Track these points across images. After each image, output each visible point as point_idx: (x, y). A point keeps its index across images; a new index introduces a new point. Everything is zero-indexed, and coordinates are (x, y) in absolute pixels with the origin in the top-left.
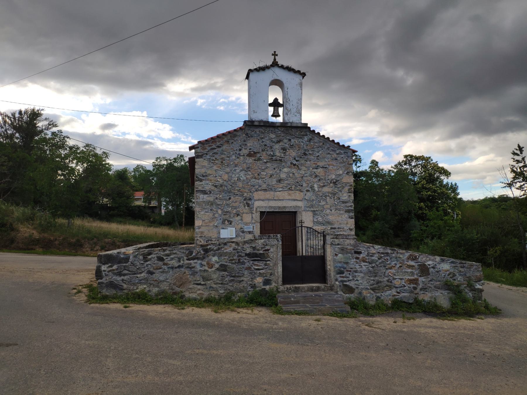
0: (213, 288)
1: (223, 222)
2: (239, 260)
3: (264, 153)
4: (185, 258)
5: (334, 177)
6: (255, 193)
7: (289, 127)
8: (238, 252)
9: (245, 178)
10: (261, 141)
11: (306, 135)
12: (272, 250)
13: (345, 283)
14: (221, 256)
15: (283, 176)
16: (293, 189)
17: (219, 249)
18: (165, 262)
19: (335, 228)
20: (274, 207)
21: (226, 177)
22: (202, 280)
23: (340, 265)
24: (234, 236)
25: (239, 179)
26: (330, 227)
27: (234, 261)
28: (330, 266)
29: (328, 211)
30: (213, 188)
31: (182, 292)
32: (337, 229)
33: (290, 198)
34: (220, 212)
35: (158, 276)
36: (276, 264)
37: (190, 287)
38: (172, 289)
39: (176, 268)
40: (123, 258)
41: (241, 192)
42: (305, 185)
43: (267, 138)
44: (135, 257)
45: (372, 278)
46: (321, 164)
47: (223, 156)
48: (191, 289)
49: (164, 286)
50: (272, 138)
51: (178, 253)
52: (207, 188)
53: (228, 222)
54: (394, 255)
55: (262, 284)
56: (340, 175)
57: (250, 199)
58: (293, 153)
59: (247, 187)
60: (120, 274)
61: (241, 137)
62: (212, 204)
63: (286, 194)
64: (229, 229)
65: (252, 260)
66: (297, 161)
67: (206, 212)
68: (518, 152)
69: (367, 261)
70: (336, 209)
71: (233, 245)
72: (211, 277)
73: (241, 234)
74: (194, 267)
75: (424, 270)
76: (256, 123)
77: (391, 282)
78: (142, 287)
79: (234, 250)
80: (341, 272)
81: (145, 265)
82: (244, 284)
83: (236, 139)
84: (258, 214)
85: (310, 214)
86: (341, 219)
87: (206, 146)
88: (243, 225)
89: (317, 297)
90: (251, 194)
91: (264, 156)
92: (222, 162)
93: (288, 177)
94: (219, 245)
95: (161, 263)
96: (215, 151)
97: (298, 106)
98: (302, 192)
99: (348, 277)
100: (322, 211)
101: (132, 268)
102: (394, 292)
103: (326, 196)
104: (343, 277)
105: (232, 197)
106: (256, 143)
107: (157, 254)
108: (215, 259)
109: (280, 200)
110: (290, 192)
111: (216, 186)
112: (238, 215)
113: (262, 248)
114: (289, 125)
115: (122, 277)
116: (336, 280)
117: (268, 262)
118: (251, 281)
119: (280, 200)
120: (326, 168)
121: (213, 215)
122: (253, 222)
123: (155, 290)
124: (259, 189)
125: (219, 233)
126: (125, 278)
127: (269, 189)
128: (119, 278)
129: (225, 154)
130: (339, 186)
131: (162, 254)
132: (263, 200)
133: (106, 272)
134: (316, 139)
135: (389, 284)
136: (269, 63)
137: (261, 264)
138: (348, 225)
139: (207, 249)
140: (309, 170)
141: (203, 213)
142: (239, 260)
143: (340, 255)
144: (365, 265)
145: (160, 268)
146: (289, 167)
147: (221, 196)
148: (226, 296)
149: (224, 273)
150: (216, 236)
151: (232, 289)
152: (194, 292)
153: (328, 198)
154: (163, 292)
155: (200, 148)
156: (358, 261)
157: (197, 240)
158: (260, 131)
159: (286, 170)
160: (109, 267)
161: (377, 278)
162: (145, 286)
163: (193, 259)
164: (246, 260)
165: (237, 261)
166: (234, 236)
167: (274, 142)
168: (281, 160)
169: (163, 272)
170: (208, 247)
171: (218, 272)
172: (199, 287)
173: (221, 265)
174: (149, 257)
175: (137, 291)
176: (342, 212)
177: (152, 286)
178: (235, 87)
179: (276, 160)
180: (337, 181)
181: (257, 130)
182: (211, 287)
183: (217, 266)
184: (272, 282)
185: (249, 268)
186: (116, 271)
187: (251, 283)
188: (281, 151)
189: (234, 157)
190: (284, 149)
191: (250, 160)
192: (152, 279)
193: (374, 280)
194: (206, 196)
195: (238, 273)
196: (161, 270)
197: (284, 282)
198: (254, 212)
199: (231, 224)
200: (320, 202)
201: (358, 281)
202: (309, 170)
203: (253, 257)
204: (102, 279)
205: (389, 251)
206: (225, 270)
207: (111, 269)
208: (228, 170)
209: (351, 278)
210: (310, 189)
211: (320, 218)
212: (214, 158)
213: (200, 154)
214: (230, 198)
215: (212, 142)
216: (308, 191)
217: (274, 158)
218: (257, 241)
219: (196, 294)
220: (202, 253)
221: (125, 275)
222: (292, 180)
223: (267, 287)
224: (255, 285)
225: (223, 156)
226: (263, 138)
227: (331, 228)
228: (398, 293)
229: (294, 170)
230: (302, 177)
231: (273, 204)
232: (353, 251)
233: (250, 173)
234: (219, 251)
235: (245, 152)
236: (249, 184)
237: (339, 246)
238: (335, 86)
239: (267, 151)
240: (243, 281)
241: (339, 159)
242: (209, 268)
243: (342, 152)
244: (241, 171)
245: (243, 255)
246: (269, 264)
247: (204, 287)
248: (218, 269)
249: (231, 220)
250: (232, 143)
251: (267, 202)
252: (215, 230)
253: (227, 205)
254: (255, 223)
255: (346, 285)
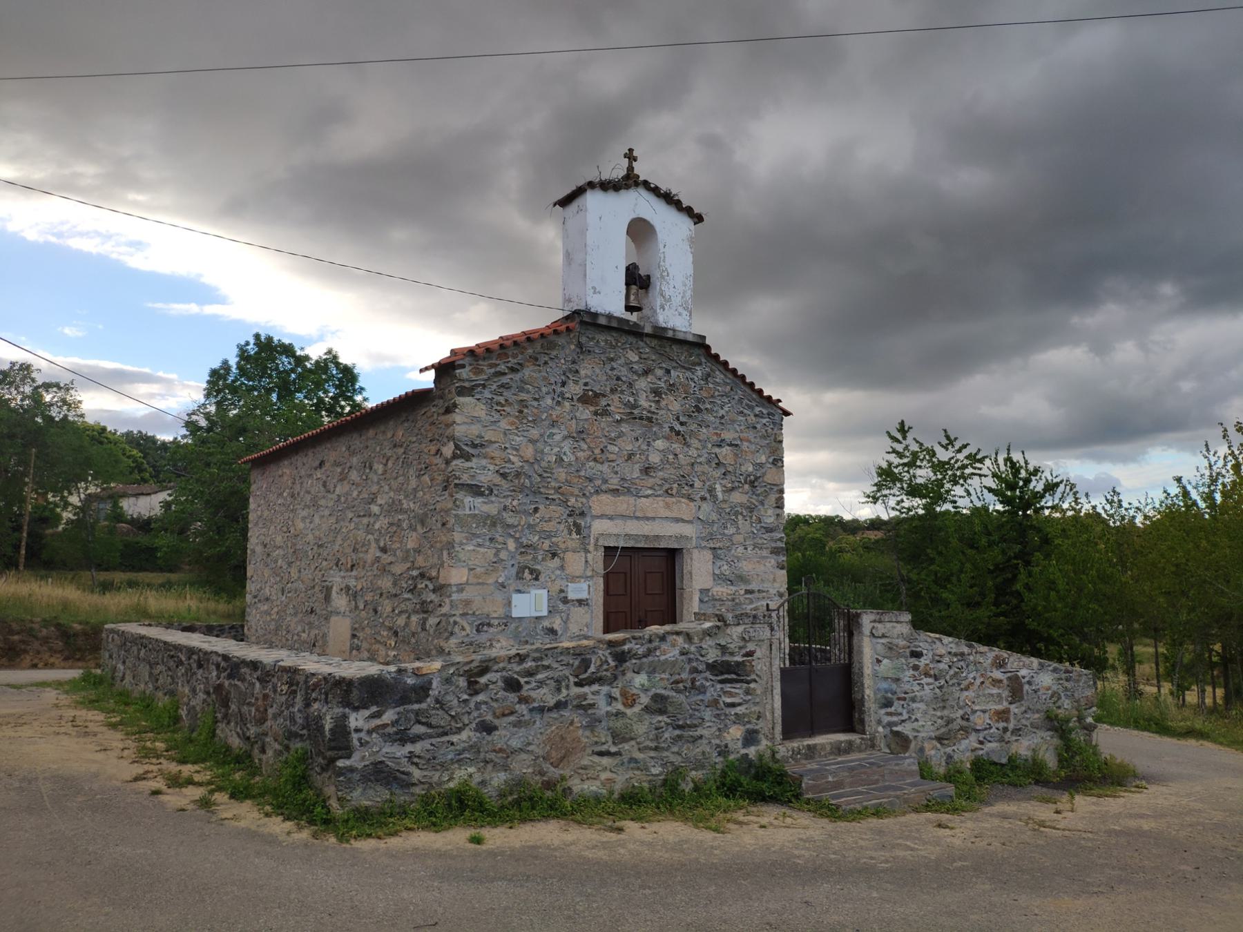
0: (636, 761)
1: (519, 576)
2: (693, 681)
3: (616, 397)
4: (572, 679)
5: (751, 469)
6: (594, 498)
7: (669, 339)
8: (690, 660)
9: (573, 458)
10: (608, 367)
11: (700, 364)
12: (758, 654)
13: (895, 729)
14: (654, 671)
15: (655, 458)
16: (674, 492)
17: (649, 652)
18: (524, 693)
19: (751, 592)
20: (636, 537)
21: (529, 452)
22: (610, 743)
23: (884, 685)
24: (545, 613)
25: (560, 460)
26: (744, 587)
27: (681, 685)
28: (870, 690)
29: (741, 549)
30: (498, 480)
31: (563, 778)
32: (757, 595)
33: (668, 514)
34: (511, 545)
35: (507, 737)
36: (769, 690)
37: (585, 762)
38: (542, 773)
39: (550, 710)
40: (414, 688)
41: (562, 494)
42: (697, 484)
43: (622, 361)
44: (448, 681)
45: (939, 714)
46: (728, 436)
47: (523, 396)
48: (585, 768)
49: (522, 767)
50: (632, 362)
51: (555, 665)
52: (486, 477)
53: (531, 573)
54: (971, 658)
55: (740, 744)
56: (761, 465)
57: (582, 514)
58: (674, 404)
59: (576, 480)
60: (403, 738)
61: (567, 352)
62: (493, 522)
63: (661, 504)
64: (534, 592)
65: (721, 682)
66: (682, 424)
67: (479, 545)
68: (899, 436)
69: (932, 672)
70: (755, 546)
71: (680, 640)
72: (632, 731)
73: (561, 606)
74: (592, 706)
75: (1016, 688)
76: (602, 321)
77: (968, 720)
78: (463, 772)
79: (682, 654)
80: (888, 704)
81: (472, 705)
82: (703, 746)
83: (554, 353)
84: (601, 553)
85: (708, 555)
86: (763, 568)
87: (484, 364)
88: (564, 583)
89: (875, 768)
90: (584, 500)
91: (616, 406)
92: (520, 412)
93: (665, 461)
94: (650, 641)
95: (513, 697)
96: (505, 380)
97: (684, 292)
98: (692, 500)
99: (901, 714)
100: (729, 549)
101: (439, 718)
102: (972, 741)
103: (736, 514)
104: (890, 714)
105: (541, 507)
106: (598, 371)
107: (504, 669)
108: (640, 679)
109: (648, 519)
110: (669, 499)
111: (504, 476)
112: (554, 555)
113: (740, 648)
114: (670, 334)
115: (409, 747)
116: (879, 722)
117: (752, 685)
118: (718, 737)
119: (648, 519)
120: (737, 445)
121: (496, 555)
122: (589, 573)
123: (498, 779)
124: (604, 487)
125: (510, 603)
126: (418, 748)
127: (624, 489)
128: (401, 751)
129: (528, 392)
130: (760, 490)
131: (518, 669)
132: (611, 518)
133: (362, 735)
134: (719, 376)
135: (964, 723)
136: (620, 173)
137: (739, 689)
138: (776, 585)
139: (623, 652)
140: (704, 447)
141: (471, 548)
142: (693, 681)
143: (885, 661)
144: (928, 684)
145: (512, 713)
146: (667, 438)
147: (515, 503)
148: (665, 781)
149: (660, 718)
150: (501, 612)
151: (677, 760)
152: (596, 778)
153: (740, 517)
154: (520, 783)
155: (468, 368)
156: (916, 673)
157: (455, 623)
158: (606, 341)
159: (660, 444)
160: (373, 716)
161: (946, 712)
162: (471, 770)
163: (590, 682)
164: (703, 679)
165: (689, 685)
166: (545, 613)
167: (635, 373)
168: (650, 420)
169: (518, 724)
170: (626, 647)
171: (646, 716)
172: (605, 761)
173: (657, 698)
174: (483, 680)
175: (451, 785)
176: (765, 553)
177: (490, 767)
178: (132, 196)
179: (641, 418)
180: (757, 478)
181: (602, 337)
182: (632, 760)
183: (645, 700)
184: (761, 736)
185: (714, 703)
186: (391, 730)
187: (718, 742)
188: (651, 396)
189: (549, 402)
190: (657, 392)
191: (585, 413)
192: (490, 747)
193: (942, 718)
194: (480, 500)
195: (691, 716)
196: (512, 718)
197: (788, 734)
198: (591, 548)
199: (537, 579)
200: (726, 528)
201: (917, 720)
202: (704, 447)
203: (722, 673)
204: (349, 757)
205: (966, 650)
206: (662, 712)
207: (378, 722)
208: (534, 433)
209: (905, 716)
210: (707, 496)
211: (726, 567)
212: (502, 399)
213: (467, 384)
214: (536, 510)
215: (499, 357)
216: (703, 499)
217: (636, 412)
218: (728, 631)
219: (598, 783)
220: (613, 664)
221: (415, 739)
222: (673, 471)
223: (752, 751)
224: (726, 746)
225: (523, 396)
226: (612, 360)
227: (747, 592)
228: (981, 743)
229: (676, 446)
230: (693, 464)
231: (634, 528)
232: (908, 651)
233: (585, 446)
234: (650, 658)
235: (574, 389)
236: (582, 473)
237: (883, 641)
238: (399, 235)
239: (622, 392)
240: (701, 737)
241: (758, 426)
242: (624, 704)
243: (765, 411)
244: (565, 438)
245: (702, 667)
246: (754, 690)
247: (617, 760)
248: (647, 709)
249: (538, 567)
250: (546, 363)
251: (619, 522)
252: (499, 597)
253: (530, 526)
254: (592, 577)
255: (897, 734)
